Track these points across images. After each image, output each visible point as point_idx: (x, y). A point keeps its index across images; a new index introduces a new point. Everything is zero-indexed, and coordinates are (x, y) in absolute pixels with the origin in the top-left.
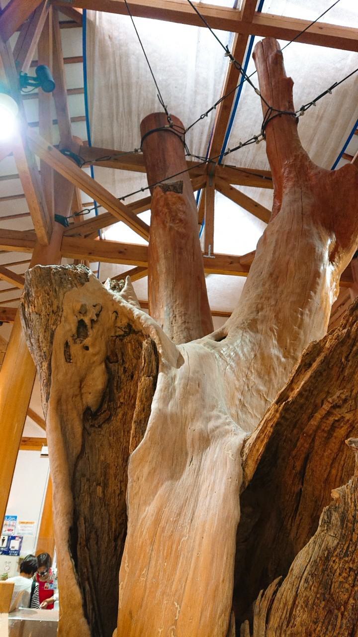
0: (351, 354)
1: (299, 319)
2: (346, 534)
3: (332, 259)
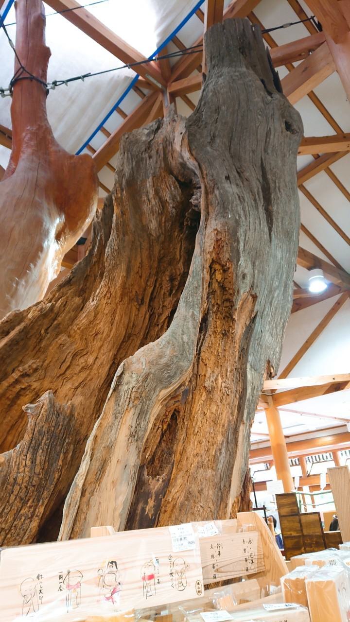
0: (51, 327)
1: (13, 289)
2: (4, 496)
3: (58, 237)
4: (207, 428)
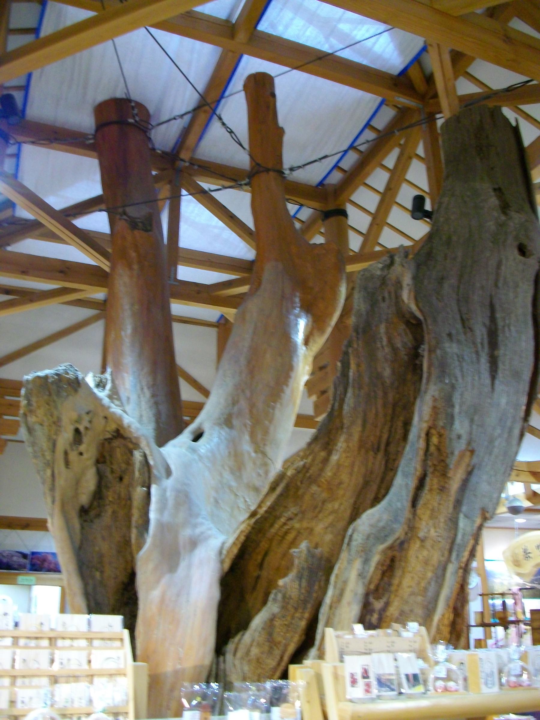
4: (419, 568)
